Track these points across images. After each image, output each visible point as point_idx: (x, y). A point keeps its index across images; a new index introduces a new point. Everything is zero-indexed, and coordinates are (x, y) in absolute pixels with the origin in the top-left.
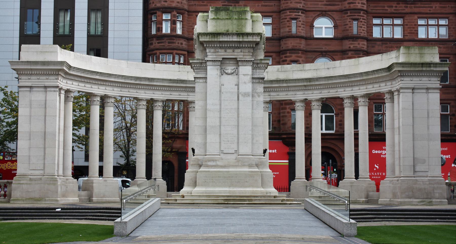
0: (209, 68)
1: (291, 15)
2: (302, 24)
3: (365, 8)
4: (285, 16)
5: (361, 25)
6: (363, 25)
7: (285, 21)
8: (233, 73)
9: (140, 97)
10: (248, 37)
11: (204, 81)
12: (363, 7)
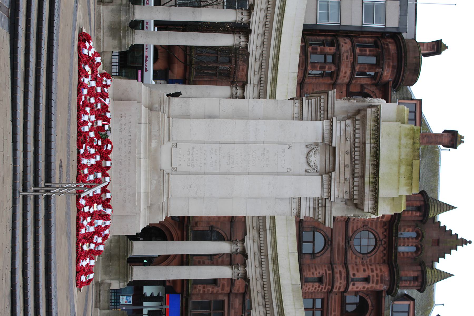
0: (319, 123)
3: (335, 290)
5: (315, 286)
6: (315, 289)
8: (309, 164)
9: (255, 13)
10: (372, 191)
11: (297, 115)
12: (336, 288)
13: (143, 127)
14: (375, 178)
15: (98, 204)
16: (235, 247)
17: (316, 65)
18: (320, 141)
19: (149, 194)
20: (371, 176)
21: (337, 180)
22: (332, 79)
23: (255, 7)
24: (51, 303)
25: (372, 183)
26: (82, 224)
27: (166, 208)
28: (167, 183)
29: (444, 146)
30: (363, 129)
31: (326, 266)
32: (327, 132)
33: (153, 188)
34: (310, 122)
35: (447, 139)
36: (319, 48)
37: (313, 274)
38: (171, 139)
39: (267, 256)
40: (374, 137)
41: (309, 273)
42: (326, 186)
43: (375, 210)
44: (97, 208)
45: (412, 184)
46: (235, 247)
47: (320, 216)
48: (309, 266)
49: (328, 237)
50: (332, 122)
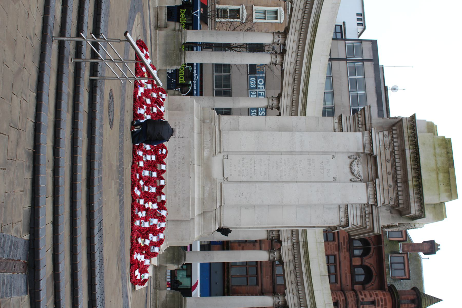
0: (359, 134)
10: (416, 194)
13: (196, 136)
14: (418, 181)
15: (153, 203)
16: (277, 300)
18: (362, 151)
19: (202, 201)
21: (381, 187)
23: (283, 94)
24: (93, 226)
25: (416, 186)
26: (137, 215)
27: (219, 218)
28: (220, 191)
29: (425, 254)
30: (400, 137)
32: (367, 142)
33: (206, 194)
34: (349, 133)
35: (426, 248)
38: (222, 150)
40: (412, 143)
42: (371, 193)
43: (422, 212)
44: (152, 206)
45: (451, 190)
46: (277, 300)
47: (368, 224)
50: (371, 132)
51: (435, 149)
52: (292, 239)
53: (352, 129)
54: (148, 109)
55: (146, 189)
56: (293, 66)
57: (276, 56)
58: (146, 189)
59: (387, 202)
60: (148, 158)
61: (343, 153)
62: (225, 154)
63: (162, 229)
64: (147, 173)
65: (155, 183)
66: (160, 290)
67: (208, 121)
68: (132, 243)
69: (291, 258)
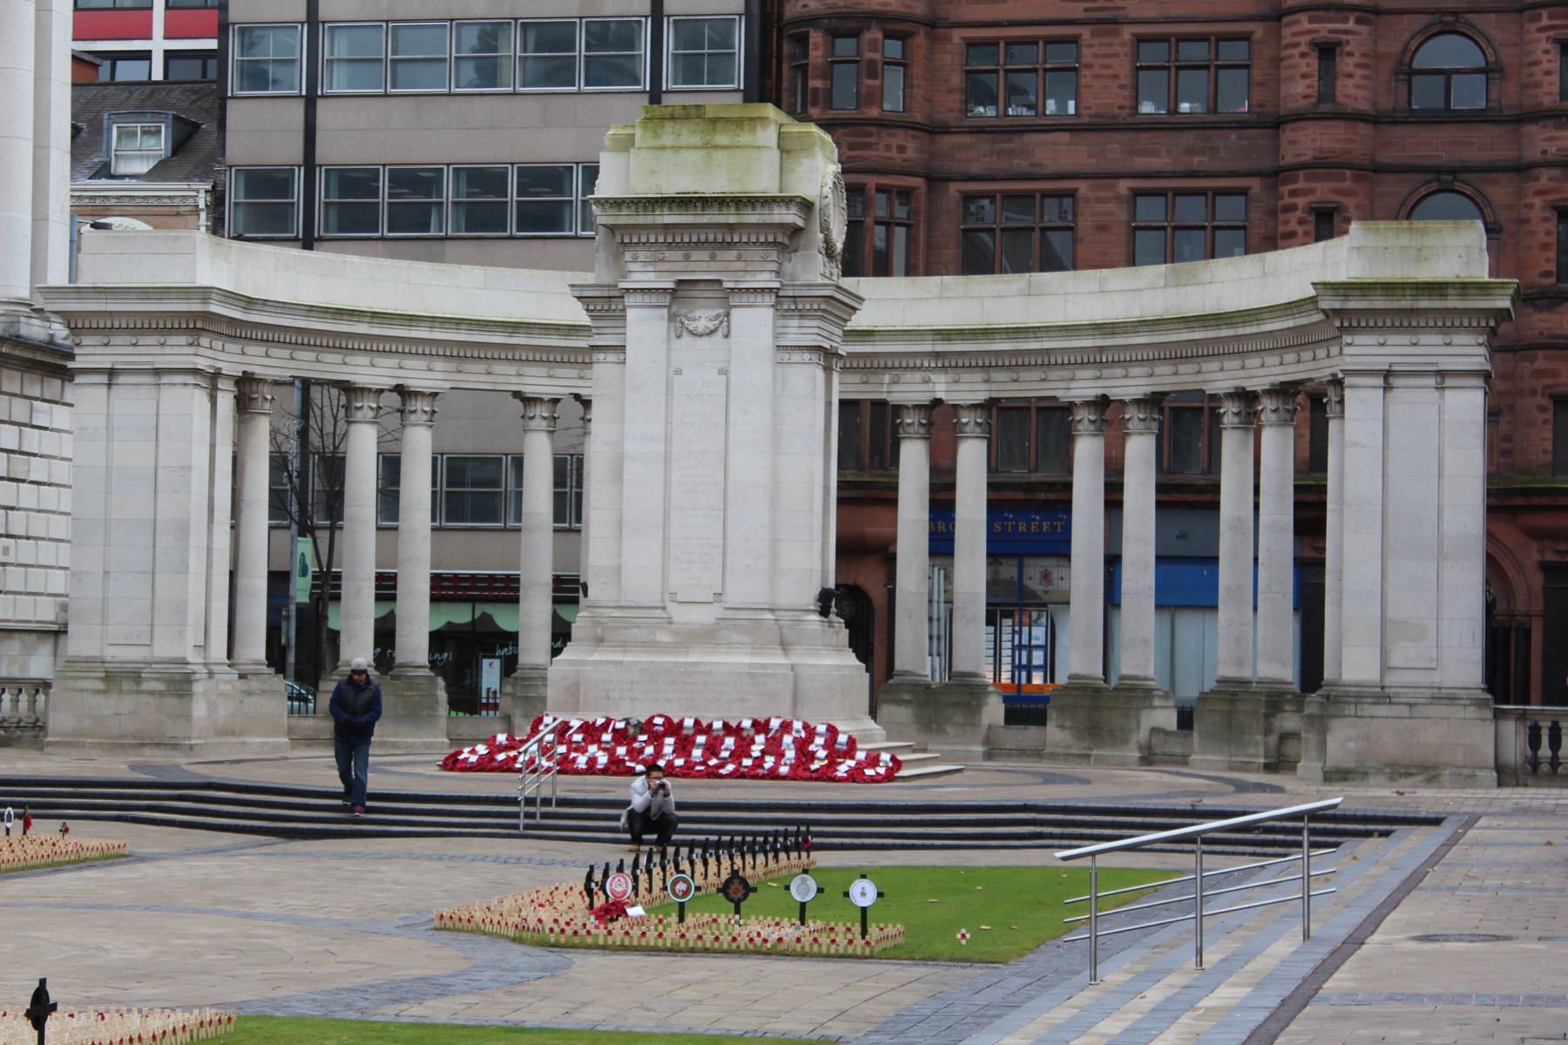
0: (631, 314)
1: (1315, 31)
2: (1358, 65)
4: (1295, 34)
7: (1291, 57)
8: (712, 332)
13: (629, 658)
15: (753, 742)
17: (864, 91)
18: (665, 311)
20: (725, 210)
22: (912, 34)
23: (514, 388)
25: (738, 209)
31: (1527, 26)
32: (647, 298)
33: (745, 639)
36: (815, 83)
37: (1548, 73)
39: (1101, 349)
41: (1546, 88)
42: (752, 298)
45: (751, 119)
48: (1527, 86)
49: (1430, 25)
51: (664, 148)
52: (929, 369)
53: (619, 323)
54: (576, 750)
55: (725, 754)
56: (439, 365)
57: (412, 412)
58: (725, 754)
59: (774, 266)
60: (668, 750)
61: (669, 349)
62: (667, 597)
63: (806, 726)
64: (697, 753)
65: (718, 737)
66: (1044, 744)
67: (599, 631)
68: (816, 779)
69: (978, 376)
